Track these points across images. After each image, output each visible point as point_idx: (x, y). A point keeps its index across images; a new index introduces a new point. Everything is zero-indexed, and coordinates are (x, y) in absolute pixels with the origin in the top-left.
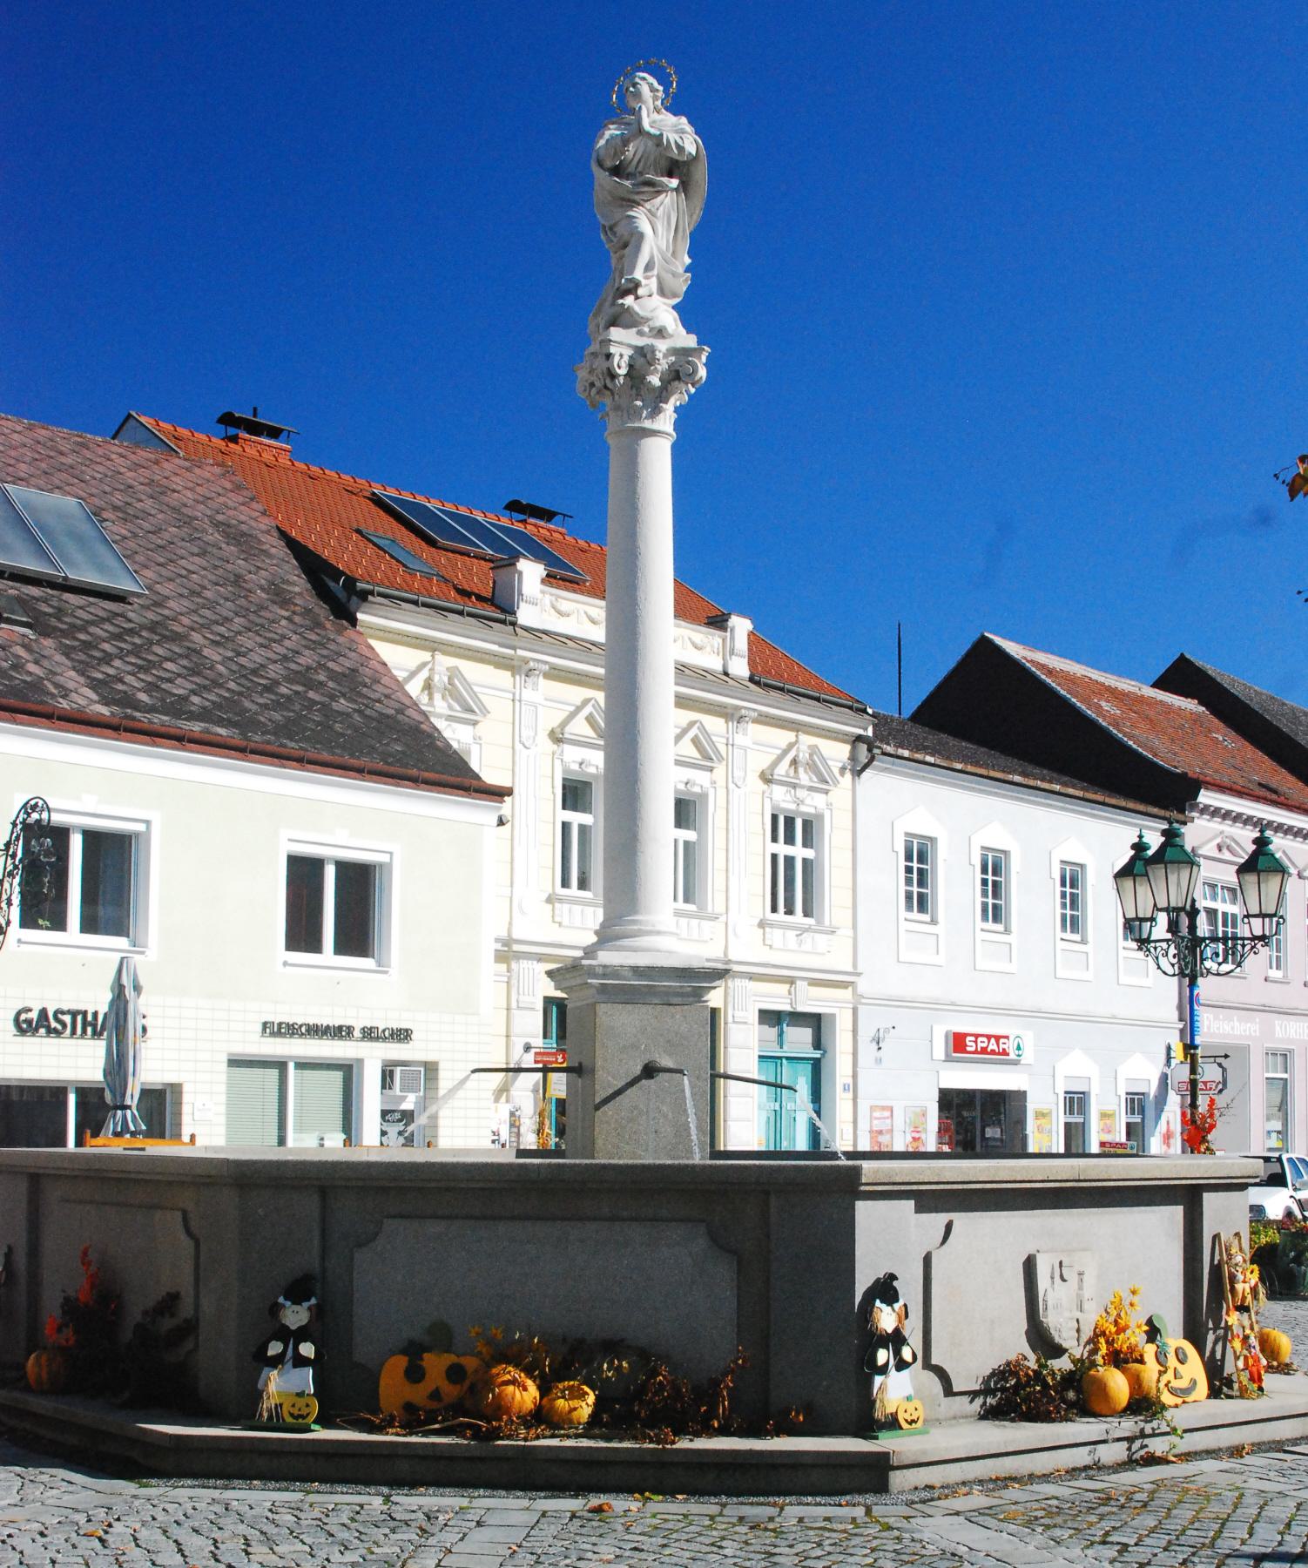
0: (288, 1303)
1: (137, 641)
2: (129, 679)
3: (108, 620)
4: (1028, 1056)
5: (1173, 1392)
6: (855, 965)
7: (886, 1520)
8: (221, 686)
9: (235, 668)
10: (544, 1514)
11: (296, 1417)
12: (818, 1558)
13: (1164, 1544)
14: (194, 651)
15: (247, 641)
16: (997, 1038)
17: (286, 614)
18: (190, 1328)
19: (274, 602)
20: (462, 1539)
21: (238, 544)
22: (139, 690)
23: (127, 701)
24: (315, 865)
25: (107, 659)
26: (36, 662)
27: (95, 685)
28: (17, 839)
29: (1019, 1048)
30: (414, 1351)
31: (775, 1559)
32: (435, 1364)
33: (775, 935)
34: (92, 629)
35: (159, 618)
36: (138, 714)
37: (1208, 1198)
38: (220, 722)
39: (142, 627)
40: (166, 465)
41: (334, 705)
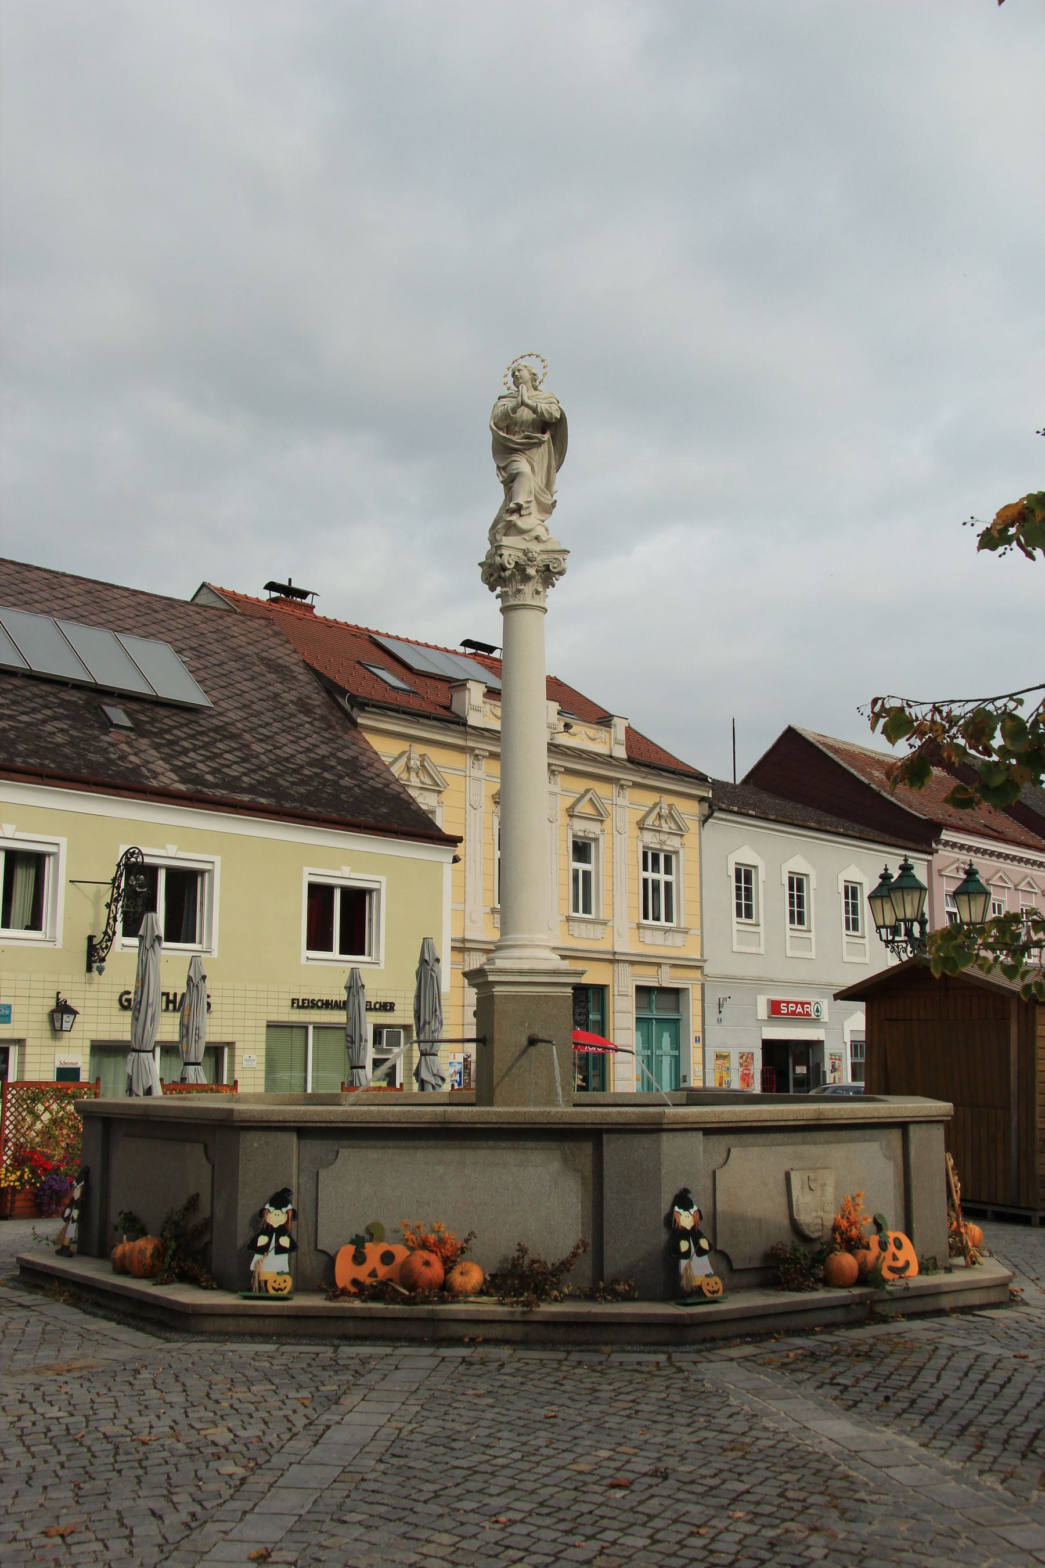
0: (272, 1209)
1: (206, 739)
2: (200, 765)
3: (186, 725)
4: (825, 1017)
5: (892, 1269)
6: (702, 955)
7: (680, 1364)
8: (263, 769)
9: (273, 757)
10: (443, 1359)
11: (277, 1290)
12: (628, 1393)
13: (874, 1386)
14: (245, 746)
15: (282, 739)
16: (803, 1004)
17: (309, 720)
18: (208, 1224)
19: (300, 712)
20: (383, 1379)
21: (276, 672)
22: (207, 773)
23: (199, 780)
24: (329, 889)
25: (185, 752)
26: (136, 754)
27: (176, 770)
28: (121, 875)
29: (817, 1011)
30: (358, 1242)
31: (597, 1394)
32: (373, 1251)
33: (648, 936)
34: (175, 732)
35: (221, 724)
36: (205, 790)
37: (912, 1128)
38: (263, 795)
39: (210, 730)
40: (227, 619)
41: (341, 782)
